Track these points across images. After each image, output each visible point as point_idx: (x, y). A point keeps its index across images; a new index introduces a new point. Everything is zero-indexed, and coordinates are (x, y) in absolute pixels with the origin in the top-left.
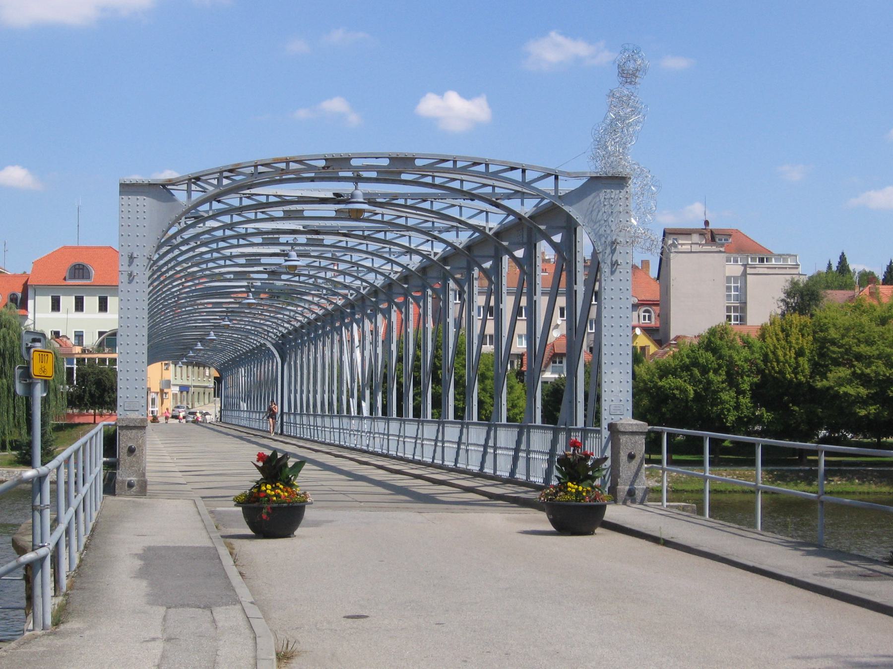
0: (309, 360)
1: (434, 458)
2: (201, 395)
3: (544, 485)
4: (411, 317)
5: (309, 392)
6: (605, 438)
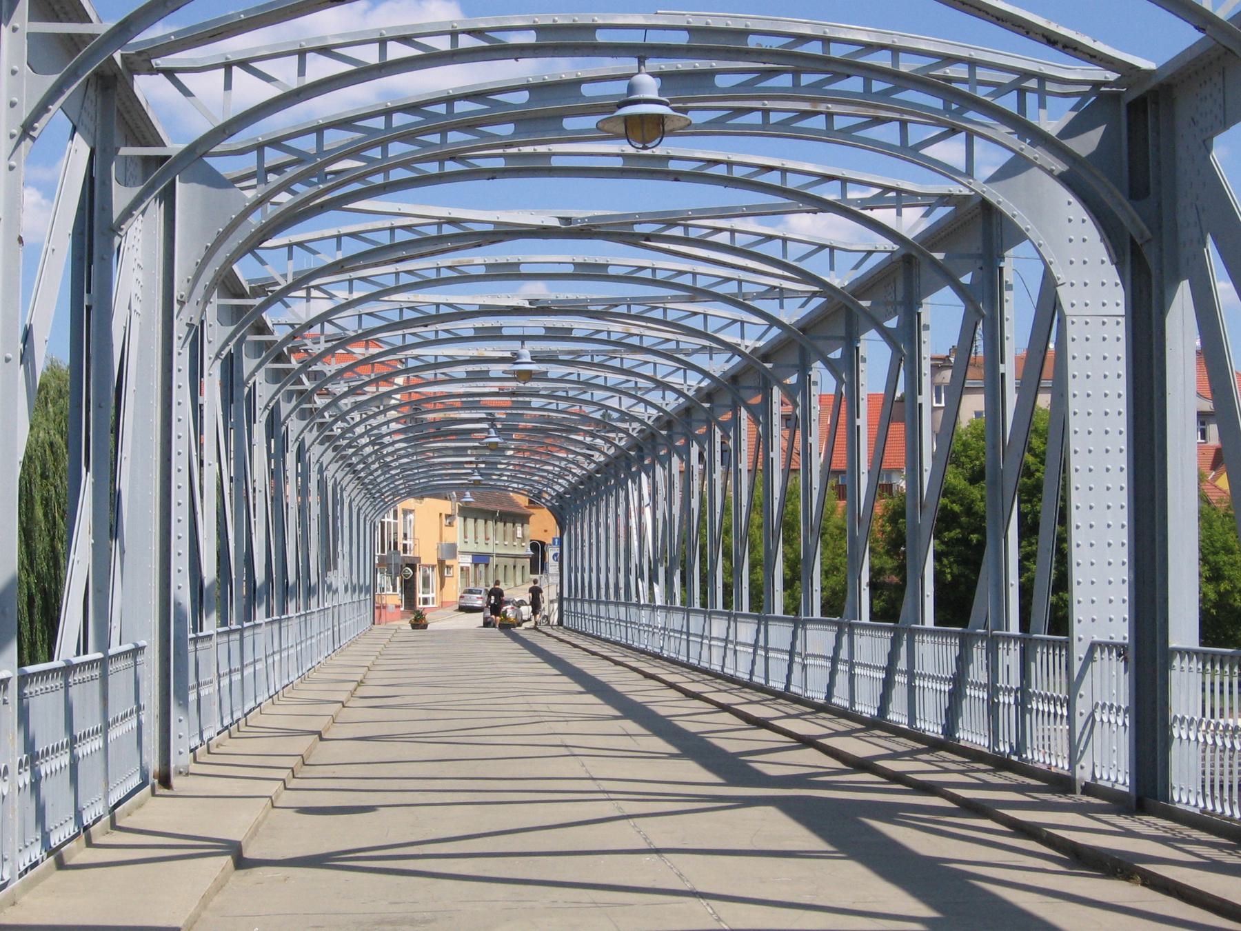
0: (617, 515)
1: (752, 673)
2: (510, 571)
3: (942, 737)
4: (744, 445)
5: (617, 570)
6: (1080, 659)
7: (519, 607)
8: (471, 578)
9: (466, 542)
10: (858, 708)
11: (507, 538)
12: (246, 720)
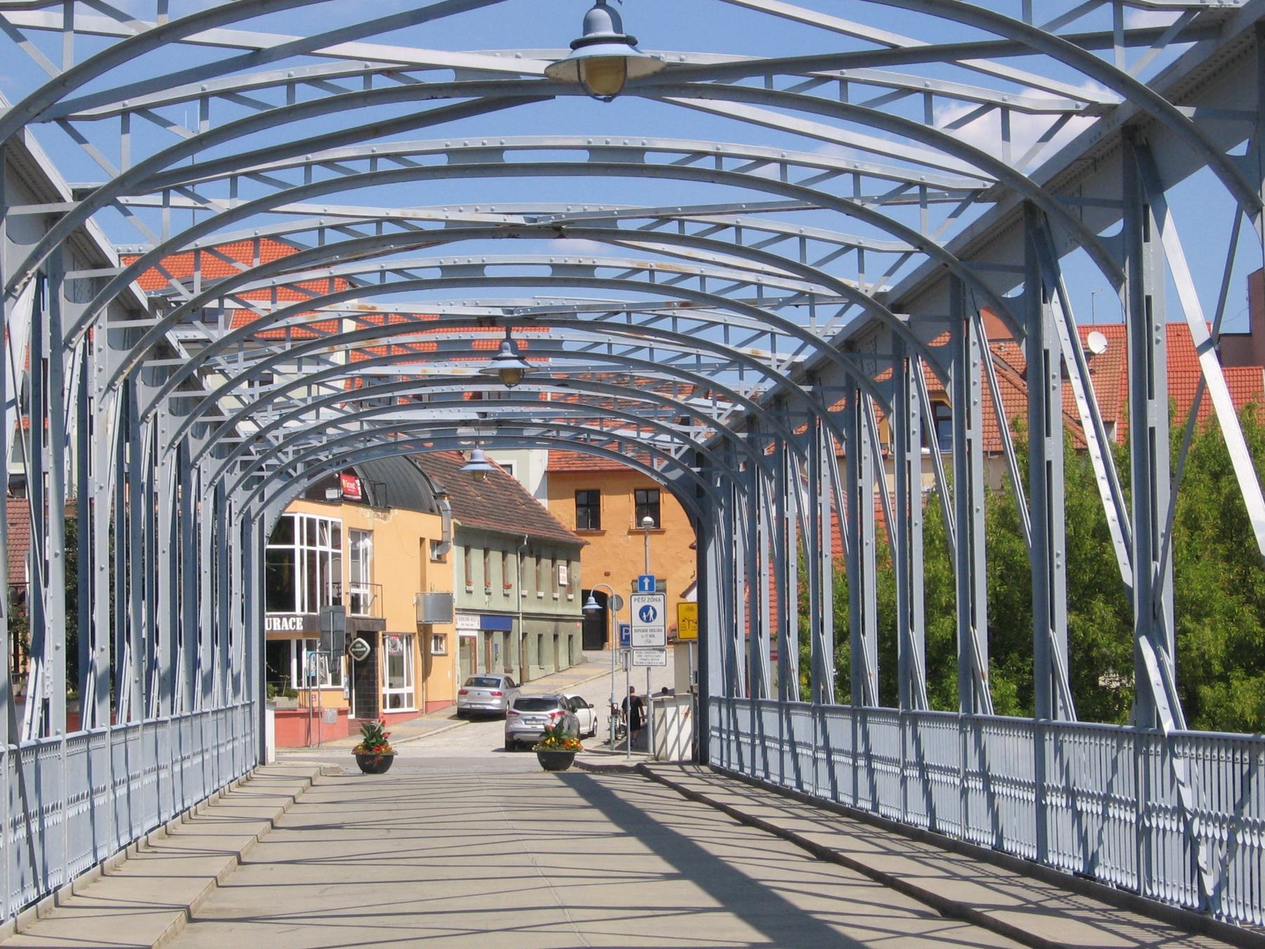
2: (548, 643)
7: (574, 711)
8: (480, 659)
9: (469, 592)
10: (1052, 858)
11: (542, 585)
12: (137, 846)
